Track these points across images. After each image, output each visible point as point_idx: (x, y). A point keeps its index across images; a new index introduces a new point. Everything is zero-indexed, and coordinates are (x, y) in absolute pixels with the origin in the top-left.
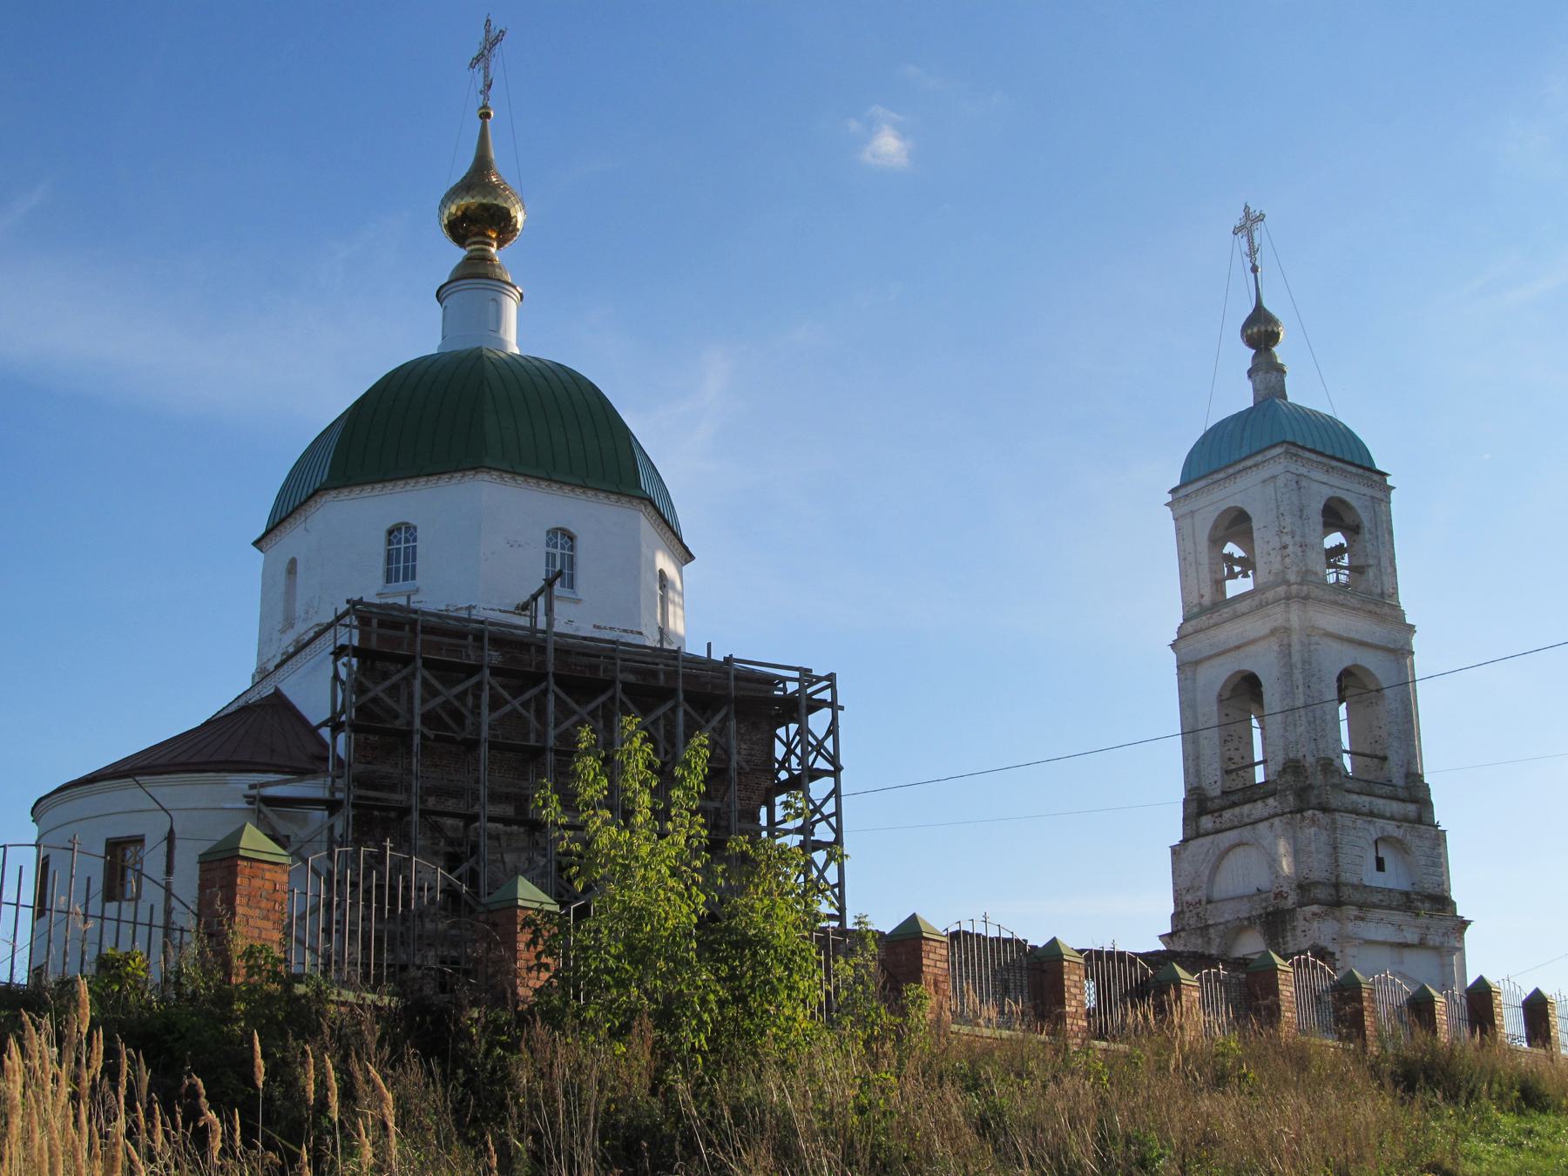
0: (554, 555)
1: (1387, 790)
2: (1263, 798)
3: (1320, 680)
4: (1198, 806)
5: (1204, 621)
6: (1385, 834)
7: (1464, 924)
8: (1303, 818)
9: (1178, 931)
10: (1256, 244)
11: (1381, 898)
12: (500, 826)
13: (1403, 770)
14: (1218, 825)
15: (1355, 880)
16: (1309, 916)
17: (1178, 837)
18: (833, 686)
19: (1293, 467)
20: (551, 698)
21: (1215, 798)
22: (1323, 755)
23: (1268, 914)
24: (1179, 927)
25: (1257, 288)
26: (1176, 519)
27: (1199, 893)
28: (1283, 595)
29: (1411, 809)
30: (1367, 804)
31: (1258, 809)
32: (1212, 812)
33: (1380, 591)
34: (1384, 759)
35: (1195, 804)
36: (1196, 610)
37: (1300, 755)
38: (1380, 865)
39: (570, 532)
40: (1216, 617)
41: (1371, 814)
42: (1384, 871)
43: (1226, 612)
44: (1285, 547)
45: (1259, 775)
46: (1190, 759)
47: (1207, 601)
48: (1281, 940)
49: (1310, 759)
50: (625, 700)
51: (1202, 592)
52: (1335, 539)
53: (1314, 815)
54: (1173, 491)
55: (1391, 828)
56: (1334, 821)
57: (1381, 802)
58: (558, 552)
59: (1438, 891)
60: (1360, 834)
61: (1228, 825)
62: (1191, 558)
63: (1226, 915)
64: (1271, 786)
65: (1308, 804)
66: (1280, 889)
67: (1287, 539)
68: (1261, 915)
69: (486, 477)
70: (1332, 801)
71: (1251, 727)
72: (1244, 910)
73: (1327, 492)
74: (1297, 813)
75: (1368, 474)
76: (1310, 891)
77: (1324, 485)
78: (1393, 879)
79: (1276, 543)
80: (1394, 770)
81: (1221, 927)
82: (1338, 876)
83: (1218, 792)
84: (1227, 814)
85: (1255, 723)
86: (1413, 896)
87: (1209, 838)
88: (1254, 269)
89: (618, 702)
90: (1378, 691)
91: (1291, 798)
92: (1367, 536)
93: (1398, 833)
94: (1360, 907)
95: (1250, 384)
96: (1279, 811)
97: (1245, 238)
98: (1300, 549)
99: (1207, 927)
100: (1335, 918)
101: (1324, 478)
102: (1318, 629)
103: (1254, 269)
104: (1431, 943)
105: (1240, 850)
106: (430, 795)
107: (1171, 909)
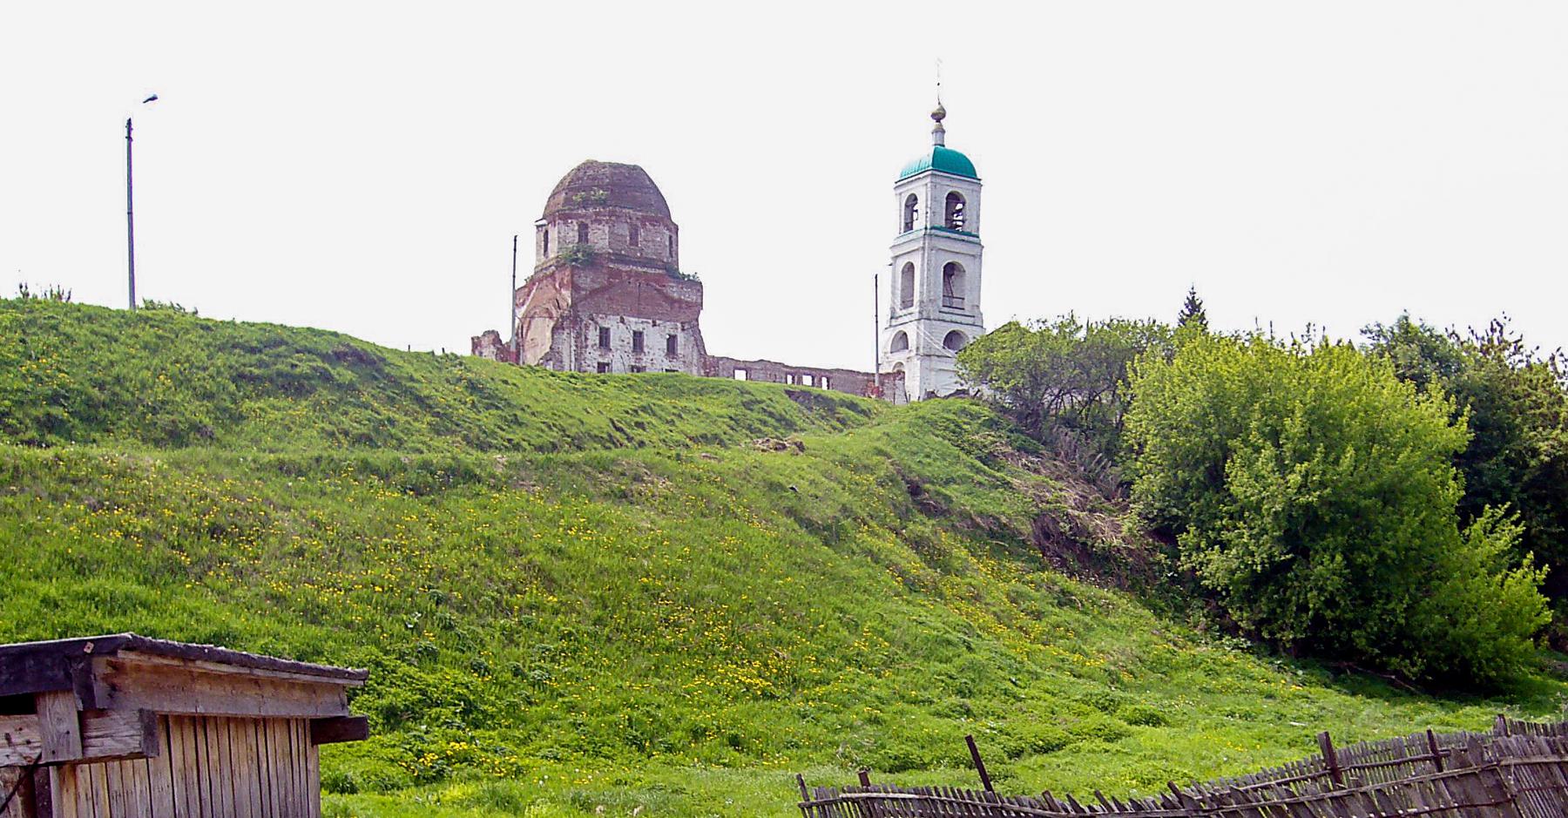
41: (952, 322)
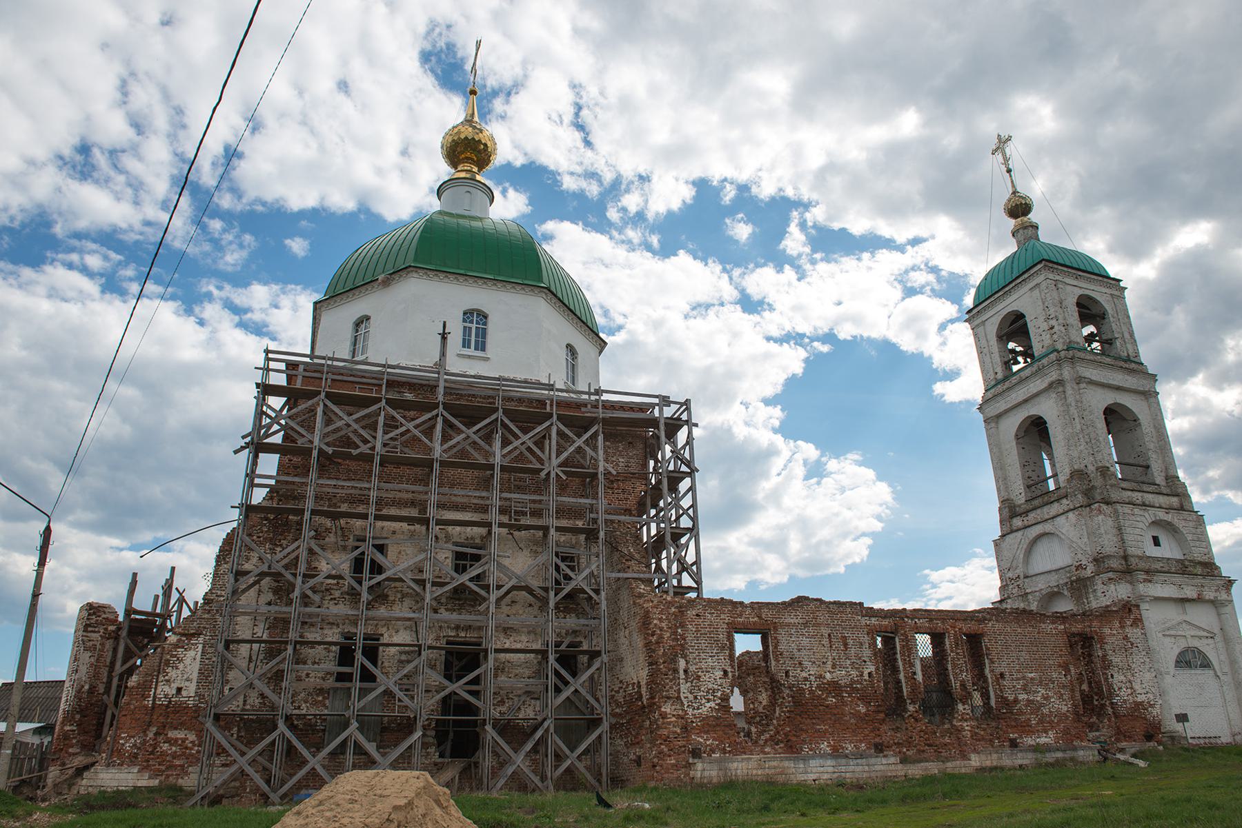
0: (470, 328)
1: (1152, 488)
2: (1058, 500)
3: (1091, 413)
4: (1010, 512)
5: (1000, 388)
6: (1158, 518)
7: (1230, 583)
8: (1092, 510)
9: (1005, 599)
10: (1008, 156)
11: (1162, 565)
12: (405, 525)
13: (1163, 474)
14: (1026, 522)
15: (1139, 553)
16: (1106, 579)
17: (997, 533)
18: (688, 409)
19: (1051, 276)
20: (440, 420)
21: (1022, 504)
22: (1100, 465)
23: (1072, 582)
24: (1006, 596)
25: (1012, 182)
26: (973, 329)
27: (1018, 571)
28: (1055, 359)
29: (1174, 501)
30: (1140, 498)
31: (1055, 509)
32: (1020, 515)
33: (1126, 355)
34: (1148, 467)
35: (1007, 510)
36: (993, 383)
37: (1082, 467)
38: (1156, 542)
39: (483, 312)
40: (1007, 384)
41: (1144, 505)
42: (1160, 546)
43: (1014, 380)
44: (1052, 328)
45: (1052, 485)
46: (1000, 480)
47: (1000, 376)
48: (1085, 600)
49: (1091, 468)
50: (507, 421)
51: (996, 371)
52: (1090, 329)
53: (1100, 506)
54: (969, 312)
55: (1161, 515)
56: (1116, 511)
57: (1150, 496)
58: (474, 326)
59: (1205, 559)
60: (1138, 519)
61: (1034, 522)
62: (985, 351)
63: (1040, 585)
64: (1062, 491)
65: (1093, 499)
66: (1080, 563)
67: (1053, 322)
68: (1067, 583)
69: (415, 275)
70: (1112, 496)
71: (1042, 460)
72: (1053, 580)
73: (1080, 292)
74: (1086, 507)
75: (1105, 280)
76: (1104, 562)
77: (1073, 290)
78: (1168, 550)
79: (1045, 326)
80: (1156, 474)
81: (1037, 594)
82: (1125, 551)
83: (1023, 501)
84: (1032, 515)
85: (1045, 456)
86: (1187, 563)
87: (1020, 533)
88: (1009, 171)
89: (565, 455)
90: (1135, 420)
91: (1080, 496)
92: (1111, 319)
93: (1168, 518)
94: (1147, 572)
95: (1014, 240)
96: (1072, 507)
97: (1000, 155)
98: (1063, 328)
99: (1026, 594)
100: (1127, 582)
101: (1075, 283)
102: (1085, 378)
103: (1009, 171)
104: (1207, 597)
105: (1045, 540)
106: (343, 502)
107: (998, 583)
